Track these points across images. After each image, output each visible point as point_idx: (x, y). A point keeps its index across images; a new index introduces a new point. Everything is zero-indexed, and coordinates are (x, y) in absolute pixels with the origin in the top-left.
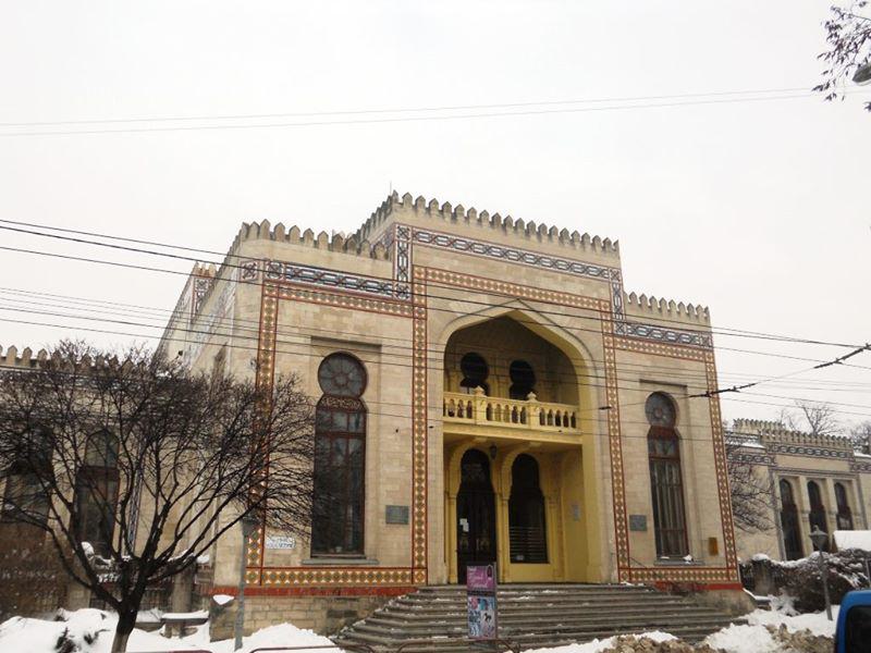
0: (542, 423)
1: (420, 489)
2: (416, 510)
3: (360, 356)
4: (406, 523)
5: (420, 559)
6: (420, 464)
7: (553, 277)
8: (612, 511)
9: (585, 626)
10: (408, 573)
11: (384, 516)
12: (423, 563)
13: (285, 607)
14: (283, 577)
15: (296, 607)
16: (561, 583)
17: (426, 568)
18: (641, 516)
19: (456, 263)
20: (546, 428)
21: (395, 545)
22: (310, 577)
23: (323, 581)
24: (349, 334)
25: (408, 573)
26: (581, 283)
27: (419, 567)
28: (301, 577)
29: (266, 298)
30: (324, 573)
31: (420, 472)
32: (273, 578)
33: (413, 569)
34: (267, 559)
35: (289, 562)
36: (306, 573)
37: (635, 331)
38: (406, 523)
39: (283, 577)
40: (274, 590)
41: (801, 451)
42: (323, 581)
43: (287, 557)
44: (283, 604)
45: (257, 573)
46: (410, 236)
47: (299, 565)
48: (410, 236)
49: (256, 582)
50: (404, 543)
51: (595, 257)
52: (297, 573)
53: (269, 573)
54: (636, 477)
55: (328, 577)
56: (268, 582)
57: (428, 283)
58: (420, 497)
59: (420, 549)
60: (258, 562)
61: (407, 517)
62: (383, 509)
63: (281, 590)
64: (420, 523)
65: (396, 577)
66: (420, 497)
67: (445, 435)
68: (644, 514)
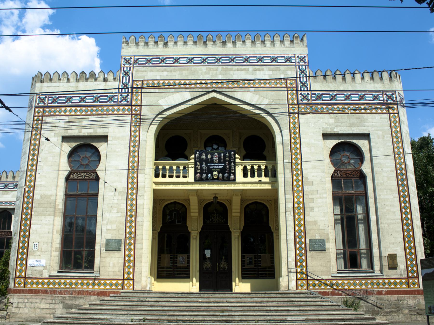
0: (245, 175)
1: (130, 227)
2: (127, 241)
3: (94, 144)
4: (120, 250)
5: (129, 274)
6: (131, 210)
7: (244, 69)
8: (293, 237)
9: (337, 317)
10: (120, 282)
11: (104, 245)
12: (131, 276)
13: (37, 301)
14: (37, 283)
15: (43, 301)
16: (141, 293)
17: (134, 279)
18: (319, 240)
19: (165, 73)
20: (249, 179)
21: (111, 265)
22: (54, 284)
23: (62, 286)
24: (85, 132)
25: (120, 282)
26: (269, 70)
27: (128, 279)
28: (49, 284)
29: (36, 118)
30: (63, 281)
31: (131, 216)
32: (32, 284)
33: (123, 279)
34: (29, 272)
35: (42, 275)
36: (51, 281)
37: (42, 100)
38: (120, 250)
39: (37, 283)
40: (83, 291)
41: (11, 186)
42: (62, 286)
43: (41, 272)
44: (36, 299)
45: (22, 280)
46: (132, 62)
47: (47, 277)
48: (132, 62)
49: (22, 285)
50: (118, 263)
51: (284, 49)
52: (46, 281)
53: (29, 281)
54: (316, 210)
55: (65, 284)
56: (29, 286)
57: (286, 89)
58: (130, 233)
59: (129, 267)
60: (23, 274)
61: (121, 246)
62: (104, 242)
63: (35, 290)
64: (130, 250)
65: (111, 285)
66: (130, 233)
67: (154, 190)
68: (322, 238)
